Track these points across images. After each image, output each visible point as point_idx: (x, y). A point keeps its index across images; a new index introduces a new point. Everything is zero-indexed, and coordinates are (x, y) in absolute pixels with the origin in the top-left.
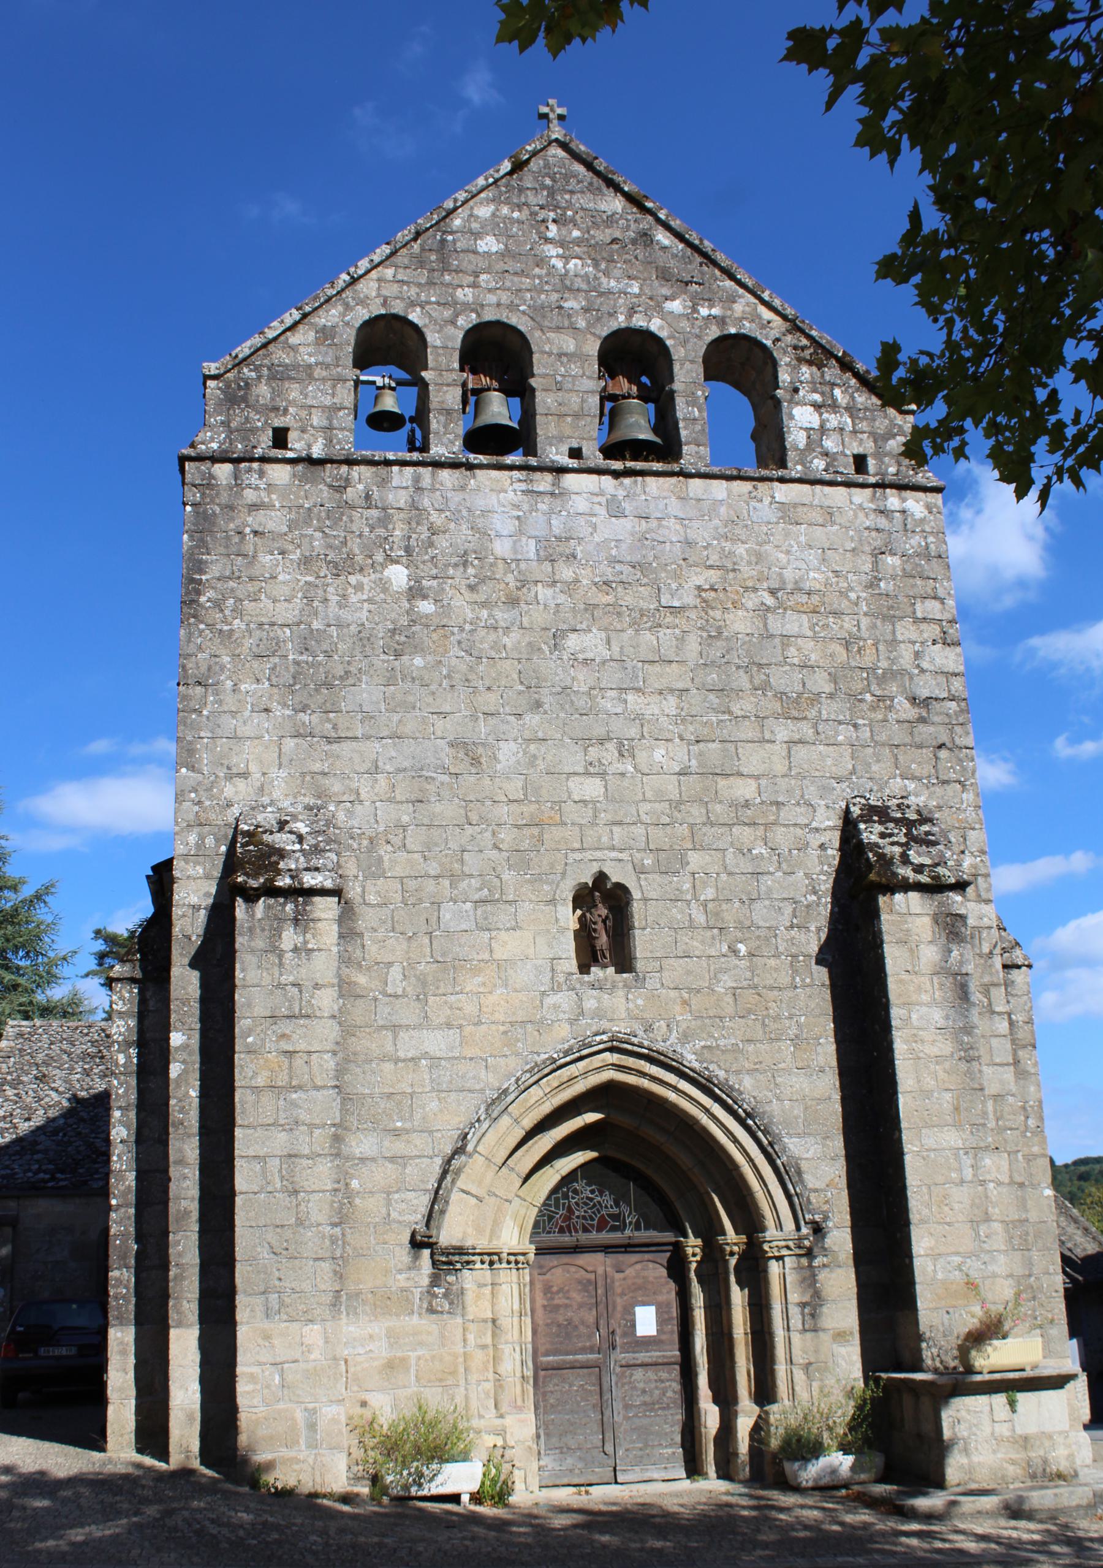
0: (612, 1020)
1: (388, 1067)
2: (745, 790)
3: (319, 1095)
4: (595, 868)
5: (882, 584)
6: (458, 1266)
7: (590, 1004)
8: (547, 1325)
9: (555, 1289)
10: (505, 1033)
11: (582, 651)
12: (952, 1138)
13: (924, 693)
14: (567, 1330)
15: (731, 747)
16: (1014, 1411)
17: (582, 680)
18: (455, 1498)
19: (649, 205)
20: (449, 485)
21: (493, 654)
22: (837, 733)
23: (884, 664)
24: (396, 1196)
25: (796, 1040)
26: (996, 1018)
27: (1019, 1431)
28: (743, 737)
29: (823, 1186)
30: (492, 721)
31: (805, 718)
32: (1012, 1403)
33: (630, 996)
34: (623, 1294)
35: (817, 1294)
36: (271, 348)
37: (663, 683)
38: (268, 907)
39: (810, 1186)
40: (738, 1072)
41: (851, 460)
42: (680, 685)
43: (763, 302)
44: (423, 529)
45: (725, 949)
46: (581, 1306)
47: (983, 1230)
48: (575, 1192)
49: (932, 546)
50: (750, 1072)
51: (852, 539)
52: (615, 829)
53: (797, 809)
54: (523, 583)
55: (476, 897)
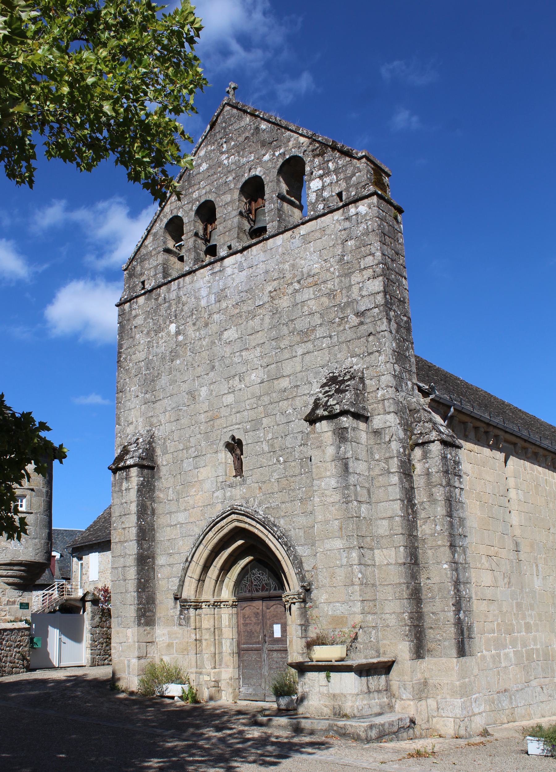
0: (235, 500)
1: (169, 528)
2: (285, 383)
4: (230, 434)
5: (345, 258)
6: (187, 607)
7: (228, 494)
8: (244, 632)
9: (246, 616)
10: (202, 510)
11: (228, 338)
12: (338, 544)
13: (363, 308)
14: (250, 634)
15: (279, 364)
16: (329, 681)
17: (228, 350)
18: (172, 698)
19: (257, 113)
21: (200, 350)
22: (322, 343)
23: (345, 300)
24: (170, 580)
25: (301, 500)
26: (391, 475)
27: (331, 692)
28: (285, 358)
29: (311, 569)
30: (200, 379)
31: (309, 340)
32: (328, 677)
33: (241, 489)
34: (269, 619)
35: (307, 620)
36: (141, 249)
37: (256, 342)
38: (119, 475)
39: (306, 569)
40: (278, 518)
41: (336, 196)
42: (262, 342)
43: (301, 135)
44: (180, 305)
46: (255, 624)
47: (350, 589)
48: (254, 574)
49: (370, 227)
51: (333, 240)
52: (238, 415)
53: (305, 387)
54: (210, 315)
55: (194, 456)
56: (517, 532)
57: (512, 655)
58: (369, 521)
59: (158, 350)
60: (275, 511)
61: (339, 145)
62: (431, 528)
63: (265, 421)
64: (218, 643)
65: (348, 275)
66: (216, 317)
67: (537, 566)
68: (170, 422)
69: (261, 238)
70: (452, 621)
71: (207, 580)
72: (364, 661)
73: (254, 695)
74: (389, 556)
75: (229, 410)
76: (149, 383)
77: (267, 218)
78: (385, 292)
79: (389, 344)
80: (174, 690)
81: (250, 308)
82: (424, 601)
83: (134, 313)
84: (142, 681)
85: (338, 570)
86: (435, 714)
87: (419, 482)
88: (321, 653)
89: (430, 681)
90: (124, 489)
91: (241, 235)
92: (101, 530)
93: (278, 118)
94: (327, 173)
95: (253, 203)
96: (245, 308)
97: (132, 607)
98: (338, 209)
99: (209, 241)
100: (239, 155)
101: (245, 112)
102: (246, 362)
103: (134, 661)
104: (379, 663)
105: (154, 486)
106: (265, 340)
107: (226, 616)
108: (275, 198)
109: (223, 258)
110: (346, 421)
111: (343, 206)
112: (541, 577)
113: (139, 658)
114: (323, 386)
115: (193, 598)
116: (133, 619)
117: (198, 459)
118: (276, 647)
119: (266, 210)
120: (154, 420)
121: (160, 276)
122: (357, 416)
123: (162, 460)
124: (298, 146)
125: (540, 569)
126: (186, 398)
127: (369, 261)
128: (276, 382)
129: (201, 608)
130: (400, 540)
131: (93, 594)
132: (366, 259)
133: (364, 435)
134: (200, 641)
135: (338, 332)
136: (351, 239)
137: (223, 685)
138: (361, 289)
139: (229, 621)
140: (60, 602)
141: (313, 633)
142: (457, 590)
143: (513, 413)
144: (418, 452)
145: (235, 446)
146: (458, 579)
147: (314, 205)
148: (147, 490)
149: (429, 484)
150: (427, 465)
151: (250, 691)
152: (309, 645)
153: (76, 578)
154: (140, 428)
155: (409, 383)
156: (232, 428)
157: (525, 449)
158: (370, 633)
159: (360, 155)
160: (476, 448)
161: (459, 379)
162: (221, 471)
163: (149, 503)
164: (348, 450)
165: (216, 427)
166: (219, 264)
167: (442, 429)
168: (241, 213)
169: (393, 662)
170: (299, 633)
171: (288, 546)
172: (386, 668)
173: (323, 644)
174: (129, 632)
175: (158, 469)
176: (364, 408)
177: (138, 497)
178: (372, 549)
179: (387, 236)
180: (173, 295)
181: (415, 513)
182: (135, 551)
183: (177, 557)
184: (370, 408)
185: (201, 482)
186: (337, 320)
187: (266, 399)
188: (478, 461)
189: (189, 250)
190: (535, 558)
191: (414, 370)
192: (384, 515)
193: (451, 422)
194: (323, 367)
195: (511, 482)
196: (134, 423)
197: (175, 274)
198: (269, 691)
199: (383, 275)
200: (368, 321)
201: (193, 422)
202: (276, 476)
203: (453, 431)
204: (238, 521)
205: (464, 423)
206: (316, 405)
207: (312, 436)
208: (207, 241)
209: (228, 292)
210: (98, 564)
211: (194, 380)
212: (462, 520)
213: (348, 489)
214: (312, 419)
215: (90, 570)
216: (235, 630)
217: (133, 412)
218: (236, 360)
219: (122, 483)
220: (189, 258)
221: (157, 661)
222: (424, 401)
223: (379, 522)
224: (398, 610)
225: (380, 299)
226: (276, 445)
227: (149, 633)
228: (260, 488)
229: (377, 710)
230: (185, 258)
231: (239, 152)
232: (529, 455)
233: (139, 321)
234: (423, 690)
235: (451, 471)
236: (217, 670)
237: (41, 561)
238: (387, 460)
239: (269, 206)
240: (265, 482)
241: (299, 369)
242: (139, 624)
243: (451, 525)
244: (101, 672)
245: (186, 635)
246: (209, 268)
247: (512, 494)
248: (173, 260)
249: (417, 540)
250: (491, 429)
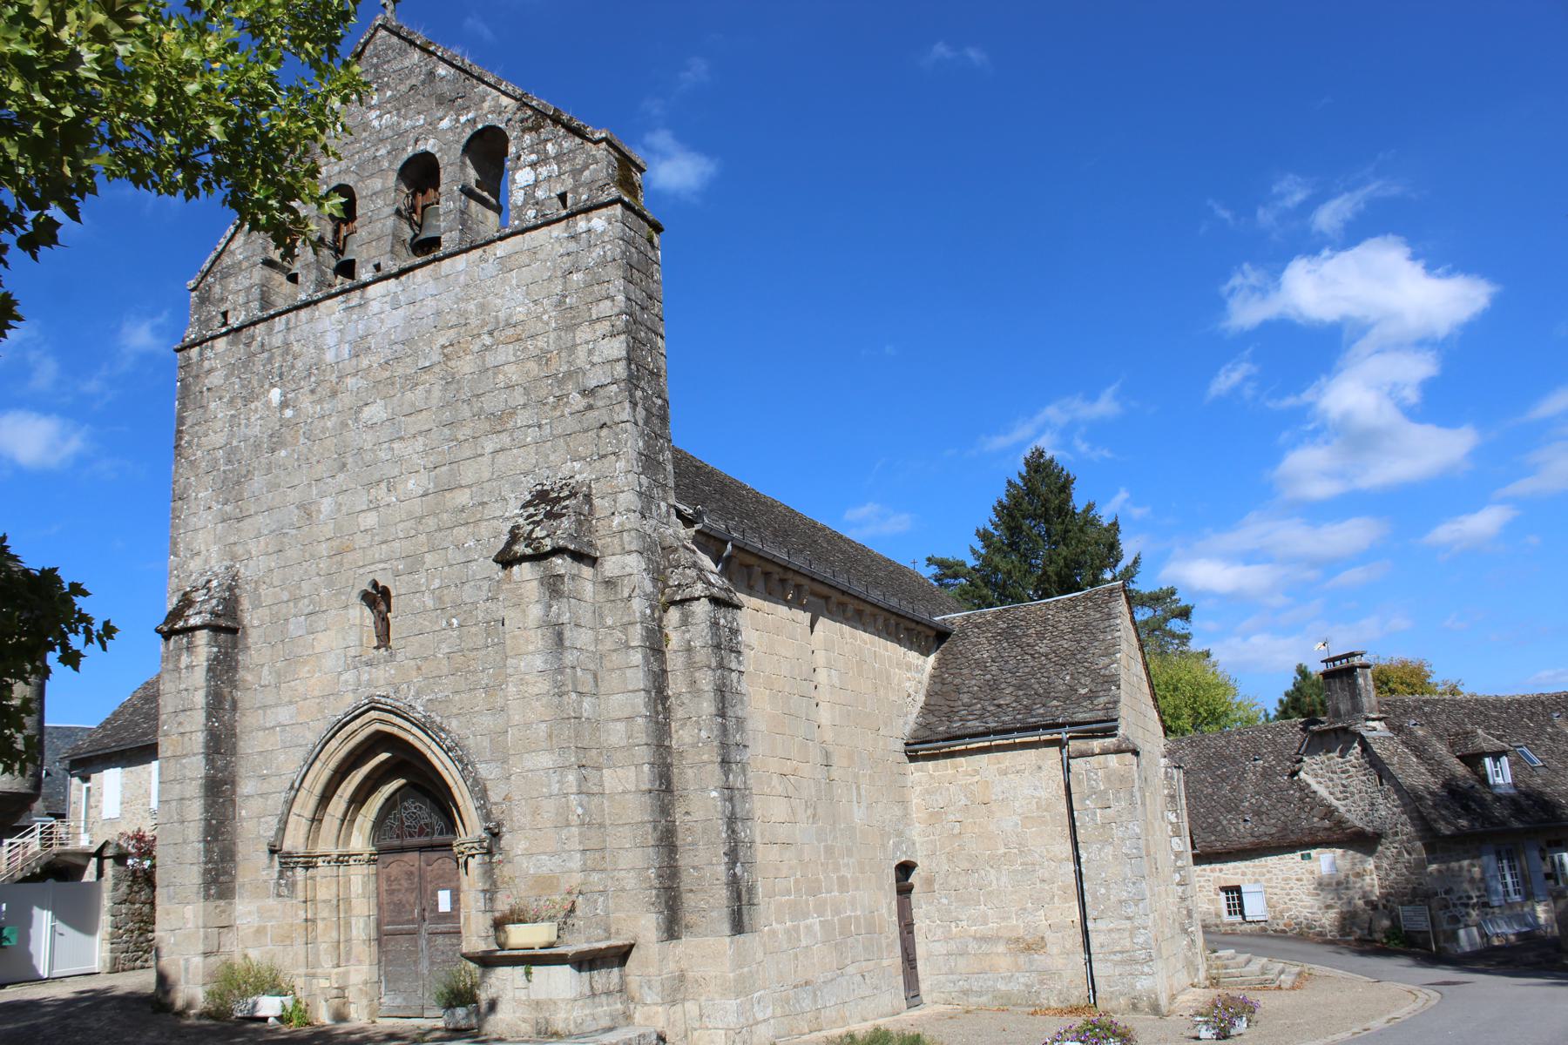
1: (261, 733)
2: (463, 498)
3: (194, 759)
7: (365, 677)
12: (546, 760)
13: (592, 383)
14: (399, 907)
17: (368, 439)
18: (265, 1019)
19: (432, 48)
23: (564, 368)
25: (486, 688)
26: (631, 652)
27: (533, 997)
30: (321, 484)
32: (528, 973)
35: (494, 883)
43: (504, 93)
44: (289, 358)
45: (444, 624)
47: (564, 833)
54: (340, 378)
56: (828, 735)
57: (817, 927)
58: (596, 724)
59: (248, 432)
60: (443, 706)
61: (565, 117)
62: (693, 732)
63: (429, 558)
64: (343, 924)
65: (571, 328)
66: (350, 382)
67: (858, 788)
68: (267, 554)
69: (431, 257)
70: (724, 879)
71: (327, 818)
72: (585, 947)
73: (405, 1008)
74: (627, 780)
75: (369, 537)
76: (232, 486)
77: (443, 225)
78: (629, 360)
79: (632, 443)
80: (269, 1006)
81: (408, 371)
82: (681, 850)
83: (206, 364)
84: (211, 994)
85: (545, 802)
86: (697, 1025)
87: (675, 661)
88: (521, 936)
89: (690, 974)
90: (183, 665)
91: (397, 247)
92: (126, 729)
93: (467, 61)
94: (544, 160)
95: (419, 195)
96: (400, 371)
97: (195, 868)
98: (559, 220)
99: (342, 253)
100: (398, 115)
101: (412, 43)
102: (399, 460)
103: (197, 961)
104: (608, 948)
105: (237, 662)
106: (433, 425)
107: (359, 879)
108: (457, 193)
109: (365, 285)
110: (560, 564)
111: (568, 217)
112: (864, 804)
113: (206, 954)
114: (524, 507)
115: (301, 850)
116: (195, 889)
117: (313, 617)
118: (442, 927)
119: (441, 211)
120: (239, 550)
121: (255, 305)
122: (578, 557)
123: (251, 617)
124: (499, 110)
125: (863, 792)
126: (295, 515)
127: (605, 307)
128: (448, 495)
129: (315, 866)
130: (644, 754)
131: (118, 845)
132: (601, 305)
133: (589, 587)
134: (314, 921)
135: (552, 419)
136: (578, 270)
137: (351, 993)
138: (590, 352)
139: (364, 888)
140: (45, 860)
141: (503, 905)
142: (732, 831)
143: (829, 542)
144: (674, 614)
145: (377, 598)
146: (733, 813)
147: (520, 210)
148: (224, 669)
149: (691, 665)
150: (687, 636)
151: (399, 1001)
152: (499, 925)
153: (77, 814)
154: (213, 562)
155: (663, 504)
156: (373, 568)
157: (842, 605)
158: (596, 901)
159: (597, 136)
160: (766, 606)
161: (744, 487)
162: (353, 639)
163: (226, 690)
164: (562, 611)
165: (346, 566)
166: (358, 293)
167: (712, 578)
168: (398, 212)
169: (632, 946)
170: (481, 904)
171: (463, 763)
172: (620, 956)
173: (521, 921)
174: (189, 911)
175: (245, 633)
176: (590, 544)
177: (208, 681)
178: (599, 769)
179: (635, 269)
180: (277, 340)
181: (667, 710)
182: (202, 773)
183: (274, 780)
184: (599, 543)
185: (319, 656)
186: (551, 399)
187: (431, 522)
188: (766, 624)
189: (307, 266)
190: (856, 776)
191: (672, 484)
192: (620, 714)
193: (727, 566)
194: (526, 474)
195: (820, 658)
196: (202, 553)
197: (282, 305)
198: (429, 999)
199: (627, 331)
200: (600, 404)
201: (307, 556)
202: (445, 649)
203: (730, 580)
204: (381, 721)
205: (749, 567)
206: (514, 536)
207: (505, 586)
208: (339, 251)
209: (372, 341)
210: (119, 788)
211: (310, 485)
212: (740, 721)
213: (562, 673)
214: (506, 560)
215: (105, 798)
216: (373, 901)
217: (201, 535)
218: (382, 455)
219: (179, 656)
220: (308, 280)
221: (238, 960)
222: (685, 534)
223: (611, 725)
224: (640, 865)
225: (620, 370)
226: (446, 599)
227: (223, 912)
228: (419, 668)
229: (605, 1022)
230: (300, 279)
231: (398, 110)
232: (849, 614)
233: (216, 379)
234: (677, 988)
235: (725, 645)
236: (341, 969)
237: (23, 791)
238: (625, 626)
239: (446, 205)
240: (426, 658)
241: (486, 475)
242: (207, 897)
243: (724, 729)
244: (140, 981)
245: (288, 913)
246: (340, 298)
247: (822, 676)
248: (280, 278)
249: (670, 754)
250: (790, 575)
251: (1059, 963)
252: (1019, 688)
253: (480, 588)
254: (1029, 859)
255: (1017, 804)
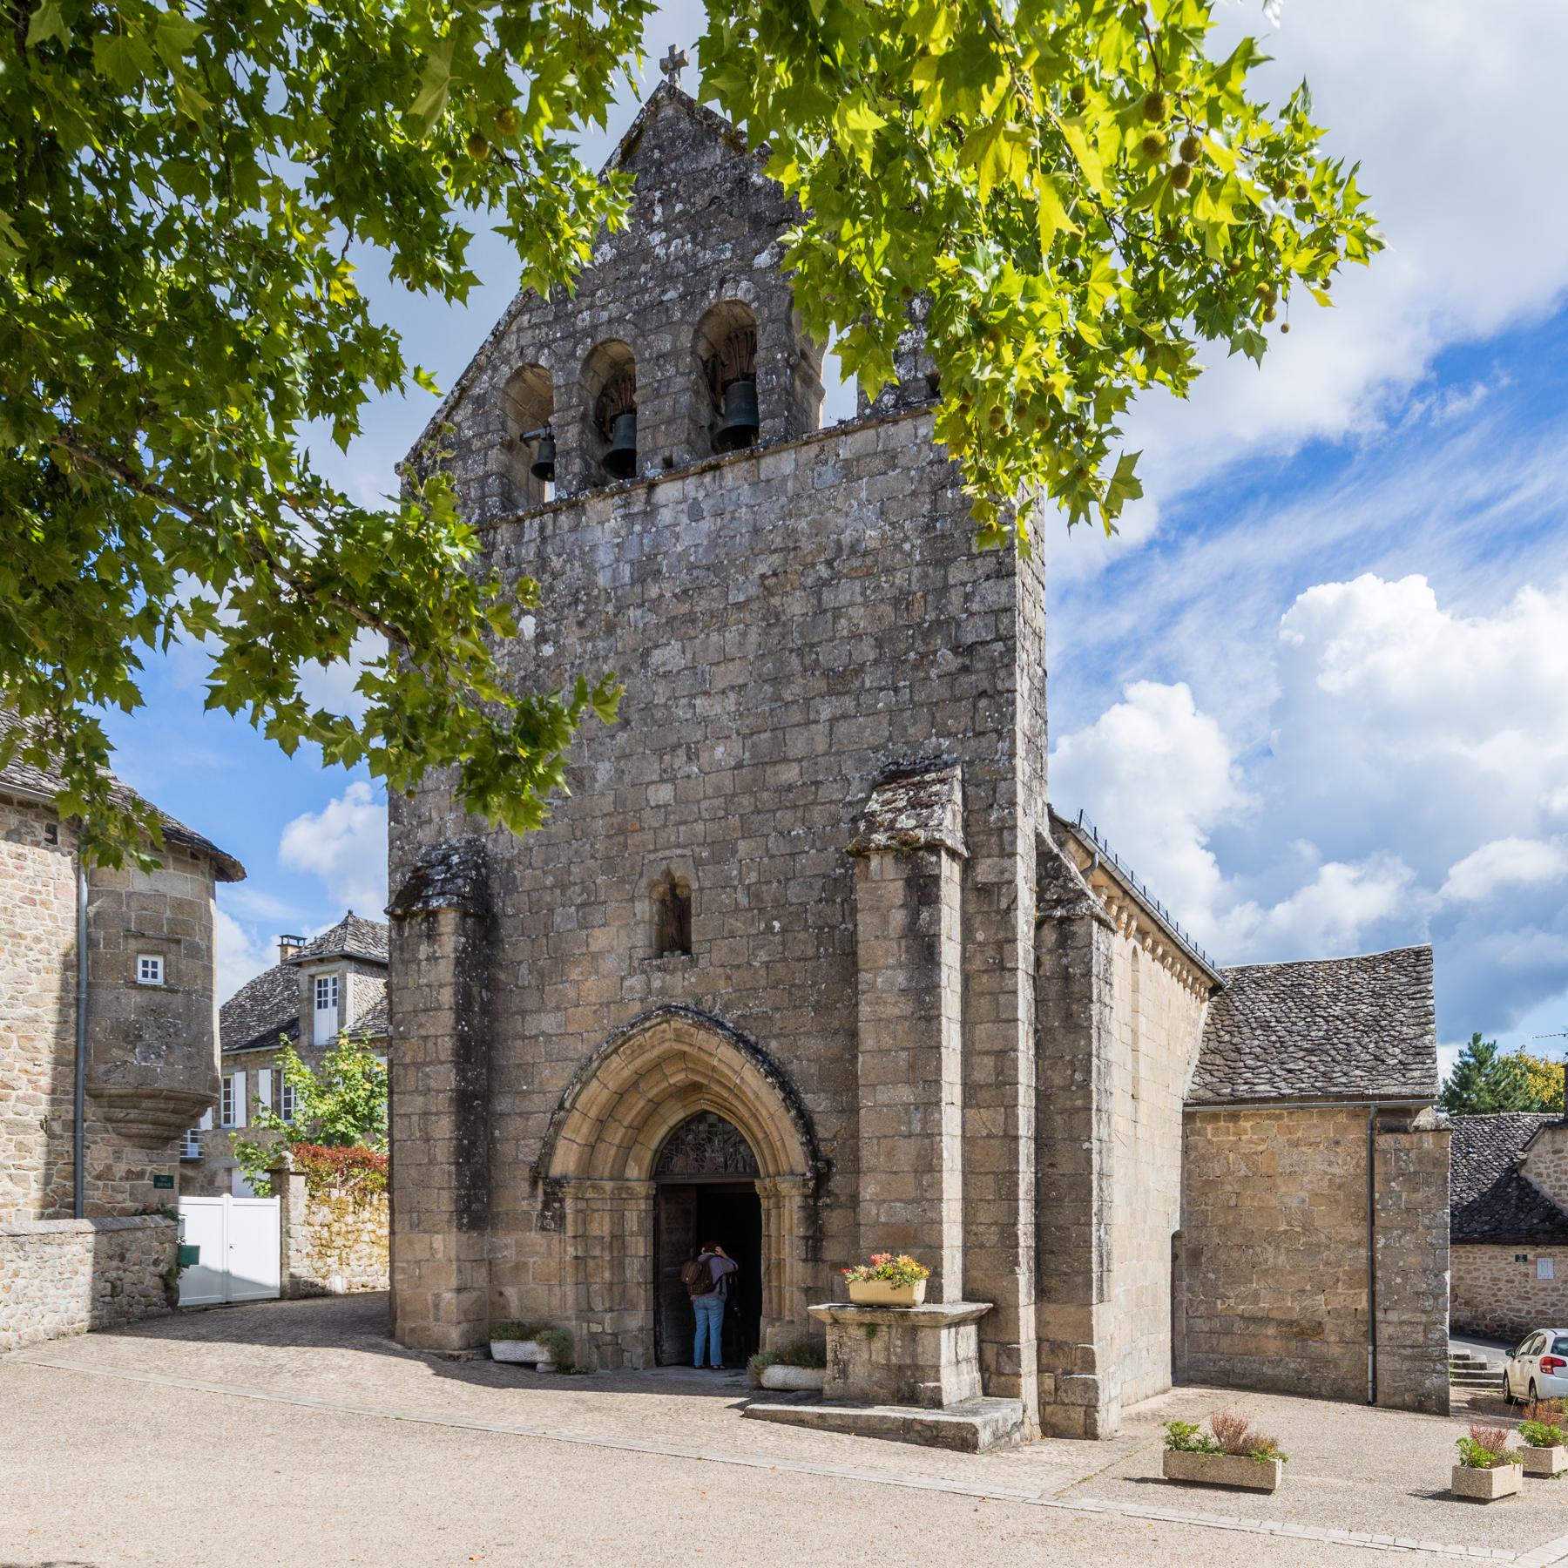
1: (519, 1042)
2: (790, 774)
7: (656, 984)
17: (661, 691)
20: (566, 528)
45: (762, 926)
50: (776, 1037)
54: (619, 610)
65: (943, 563)
66: (633, 614)
85: (901, 1142)
96: (702, 605)
100: (694, 240)
102: (705, 721)
128: (769, 770)
138: (968, 598)
150: (1065, 961)
156: (668, 853)
165: (631, 849)
192: (987, 1047)
194: (876, 750)
200: (979, 666)
201: (578, 833)
202: (763, 956)
226: (766, 897)
240: (738, 966)
251: (1336, 1351)
252: (1310, 1052)
253: (811, 887)
254: (1314, 1239)
255: (1306, 1179)
